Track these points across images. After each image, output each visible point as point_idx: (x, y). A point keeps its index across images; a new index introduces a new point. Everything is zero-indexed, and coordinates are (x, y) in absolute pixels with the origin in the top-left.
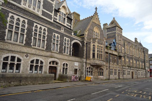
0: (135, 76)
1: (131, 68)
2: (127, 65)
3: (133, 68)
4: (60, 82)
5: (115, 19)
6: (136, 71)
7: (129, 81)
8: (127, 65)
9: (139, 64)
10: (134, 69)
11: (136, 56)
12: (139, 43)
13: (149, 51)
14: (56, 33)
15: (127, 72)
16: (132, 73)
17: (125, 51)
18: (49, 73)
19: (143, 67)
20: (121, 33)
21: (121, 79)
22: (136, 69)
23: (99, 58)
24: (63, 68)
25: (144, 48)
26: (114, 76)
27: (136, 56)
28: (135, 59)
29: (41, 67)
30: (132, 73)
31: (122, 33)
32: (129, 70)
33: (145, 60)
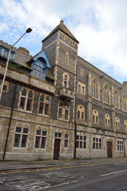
0: (116, 151)
1: (106, 133)
2: (117, 130)
3: (110, 133)
4: (16, 164)
5: (64, 23)
6: (122, 140)
7: (89, 164)
8: (117, 130)
9: (111, 121)
10: (114, 134)
11: (121, 108)
15: (90, 142)
16: (110, 144)
17: (87, 91)
20: (74, 50)
21: (64, 159)
22: (119, 134)
23: (25, 107)
26: (30, 149)
27: (121, 108)
28: (93, 105)
30: (110, 144)
31: (76, 48)
32: (99, 137)
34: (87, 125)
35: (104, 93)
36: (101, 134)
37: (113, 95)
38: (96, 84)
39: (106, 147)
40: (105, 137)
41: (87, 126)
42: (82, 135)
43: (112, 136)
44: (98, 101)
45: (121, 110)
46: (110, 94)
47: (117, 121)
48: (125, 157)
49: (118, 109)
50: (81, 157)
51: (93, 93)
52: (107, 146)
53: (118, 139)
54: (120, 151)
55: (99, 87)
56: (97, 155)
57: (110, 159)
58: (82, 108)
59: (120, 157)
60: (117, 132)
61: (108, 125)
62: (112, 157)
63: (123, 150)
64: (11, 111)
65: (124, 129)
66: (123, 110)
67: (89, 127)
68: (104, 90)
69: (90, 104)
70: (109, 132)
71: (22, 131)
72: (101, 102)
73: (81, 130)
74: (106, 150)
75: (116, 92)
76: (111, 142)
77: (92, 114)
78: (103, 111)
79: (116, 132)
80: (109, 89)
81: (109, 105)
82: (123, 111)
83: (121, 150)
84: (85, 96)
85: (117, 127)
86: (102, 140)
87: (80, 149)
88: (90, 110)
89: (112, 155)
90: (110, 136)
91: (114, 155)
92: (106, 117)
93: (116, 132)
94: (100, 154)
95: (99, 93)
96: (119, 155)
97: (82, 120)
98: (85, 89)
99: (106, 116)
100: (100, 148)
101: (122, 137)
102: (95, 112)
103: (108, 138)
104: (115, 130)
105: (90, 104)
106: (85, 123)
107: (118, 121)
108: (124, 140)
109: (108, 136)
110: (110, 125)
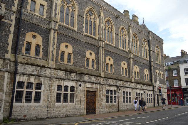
1: (86, 78)
6: (114, 89)
12: (142, 25)
13: (164, 42)
14: (38, 33)
15: (51, 91)
16: (91, 96)
17: (50, 11)
18: (116, 103)
19: (147, 80)
24: (123, 97)
25: (149, 32)
28: (106, 50)
29: (38, 95)
30: (91, 96)
32: (70, 84)
33: (152, 63)
34: (46, 65)
35: (120, 37)
36: (75, 80)
37: (131, 40)
38: (71, 5)
39: (84, 99)
40: (83, 84)
41: (45, 67)
42: (32, 80)
43: (96, 83)
44: (74, 31)
45: (116, 48)
46: (98, 22)
47: (135, 70)
48: (118, 111)
49: (111, 46)
50: (28, 116)
51: (122, 43)
52: (87, 97)
53: (107, 88)
54: (110, 103)
55: (77, 9)
56: (63, 112)
57: (92, 116)
58: (68, 47)
59: (110, 112)
60: (107, 76)
61: (124, 75)
62: (95, 113)
63: (115, 102)
64: (15, 63)
65: (120, 74)
66: (120, 48)
67: (49, 68)
68: (120, 33)
69: (103, 50)
70: (90, 76)
71: (63, 89)
72: (79, 32)
73: (30, 73)
74: (83, 104)
75: (109, 22)
76: (96, 92)
77: (105, 62)
78: (83, 47)
79: (105, 78)
80: (97, 16)
81: (95, 39)
82: (120, 49)
83: (111, 102)
84: (44, 19)
85: (135, 77)
86: (75, 89)
87: (26, 104)
88: (54, 43)
89: (95, 110)
90: (93, 83)
91: (98, 110)
92: (123, 66)
93: (105, 78)
94: (70, 109)
95: (76, 19)
96: (107, 109)
97: (35, 56)
98: (46, 8)
99: (88, 53)
100: (72, 101)
101: (114, 84)
102: (109, 59)
103: (89, 85)
104: (103, 75)
105: (55, 32)
106: (42, 62)
107: (137, 70)
108: (118, 88)
109: (88, 82)
110: (95, 67)
